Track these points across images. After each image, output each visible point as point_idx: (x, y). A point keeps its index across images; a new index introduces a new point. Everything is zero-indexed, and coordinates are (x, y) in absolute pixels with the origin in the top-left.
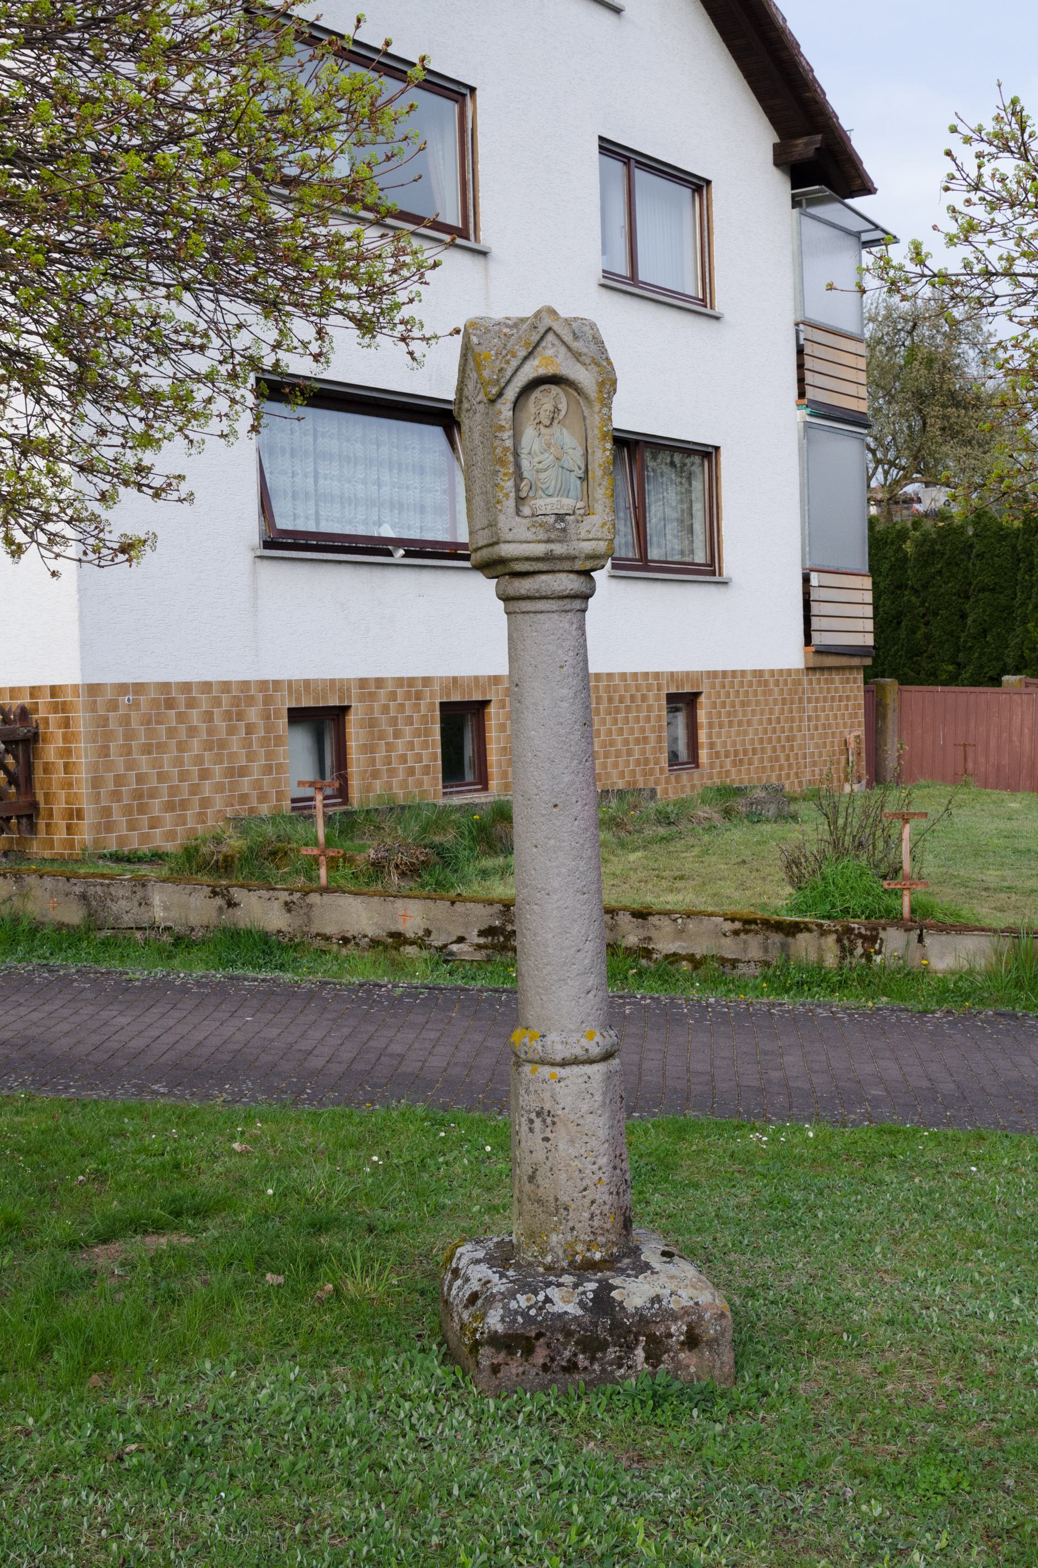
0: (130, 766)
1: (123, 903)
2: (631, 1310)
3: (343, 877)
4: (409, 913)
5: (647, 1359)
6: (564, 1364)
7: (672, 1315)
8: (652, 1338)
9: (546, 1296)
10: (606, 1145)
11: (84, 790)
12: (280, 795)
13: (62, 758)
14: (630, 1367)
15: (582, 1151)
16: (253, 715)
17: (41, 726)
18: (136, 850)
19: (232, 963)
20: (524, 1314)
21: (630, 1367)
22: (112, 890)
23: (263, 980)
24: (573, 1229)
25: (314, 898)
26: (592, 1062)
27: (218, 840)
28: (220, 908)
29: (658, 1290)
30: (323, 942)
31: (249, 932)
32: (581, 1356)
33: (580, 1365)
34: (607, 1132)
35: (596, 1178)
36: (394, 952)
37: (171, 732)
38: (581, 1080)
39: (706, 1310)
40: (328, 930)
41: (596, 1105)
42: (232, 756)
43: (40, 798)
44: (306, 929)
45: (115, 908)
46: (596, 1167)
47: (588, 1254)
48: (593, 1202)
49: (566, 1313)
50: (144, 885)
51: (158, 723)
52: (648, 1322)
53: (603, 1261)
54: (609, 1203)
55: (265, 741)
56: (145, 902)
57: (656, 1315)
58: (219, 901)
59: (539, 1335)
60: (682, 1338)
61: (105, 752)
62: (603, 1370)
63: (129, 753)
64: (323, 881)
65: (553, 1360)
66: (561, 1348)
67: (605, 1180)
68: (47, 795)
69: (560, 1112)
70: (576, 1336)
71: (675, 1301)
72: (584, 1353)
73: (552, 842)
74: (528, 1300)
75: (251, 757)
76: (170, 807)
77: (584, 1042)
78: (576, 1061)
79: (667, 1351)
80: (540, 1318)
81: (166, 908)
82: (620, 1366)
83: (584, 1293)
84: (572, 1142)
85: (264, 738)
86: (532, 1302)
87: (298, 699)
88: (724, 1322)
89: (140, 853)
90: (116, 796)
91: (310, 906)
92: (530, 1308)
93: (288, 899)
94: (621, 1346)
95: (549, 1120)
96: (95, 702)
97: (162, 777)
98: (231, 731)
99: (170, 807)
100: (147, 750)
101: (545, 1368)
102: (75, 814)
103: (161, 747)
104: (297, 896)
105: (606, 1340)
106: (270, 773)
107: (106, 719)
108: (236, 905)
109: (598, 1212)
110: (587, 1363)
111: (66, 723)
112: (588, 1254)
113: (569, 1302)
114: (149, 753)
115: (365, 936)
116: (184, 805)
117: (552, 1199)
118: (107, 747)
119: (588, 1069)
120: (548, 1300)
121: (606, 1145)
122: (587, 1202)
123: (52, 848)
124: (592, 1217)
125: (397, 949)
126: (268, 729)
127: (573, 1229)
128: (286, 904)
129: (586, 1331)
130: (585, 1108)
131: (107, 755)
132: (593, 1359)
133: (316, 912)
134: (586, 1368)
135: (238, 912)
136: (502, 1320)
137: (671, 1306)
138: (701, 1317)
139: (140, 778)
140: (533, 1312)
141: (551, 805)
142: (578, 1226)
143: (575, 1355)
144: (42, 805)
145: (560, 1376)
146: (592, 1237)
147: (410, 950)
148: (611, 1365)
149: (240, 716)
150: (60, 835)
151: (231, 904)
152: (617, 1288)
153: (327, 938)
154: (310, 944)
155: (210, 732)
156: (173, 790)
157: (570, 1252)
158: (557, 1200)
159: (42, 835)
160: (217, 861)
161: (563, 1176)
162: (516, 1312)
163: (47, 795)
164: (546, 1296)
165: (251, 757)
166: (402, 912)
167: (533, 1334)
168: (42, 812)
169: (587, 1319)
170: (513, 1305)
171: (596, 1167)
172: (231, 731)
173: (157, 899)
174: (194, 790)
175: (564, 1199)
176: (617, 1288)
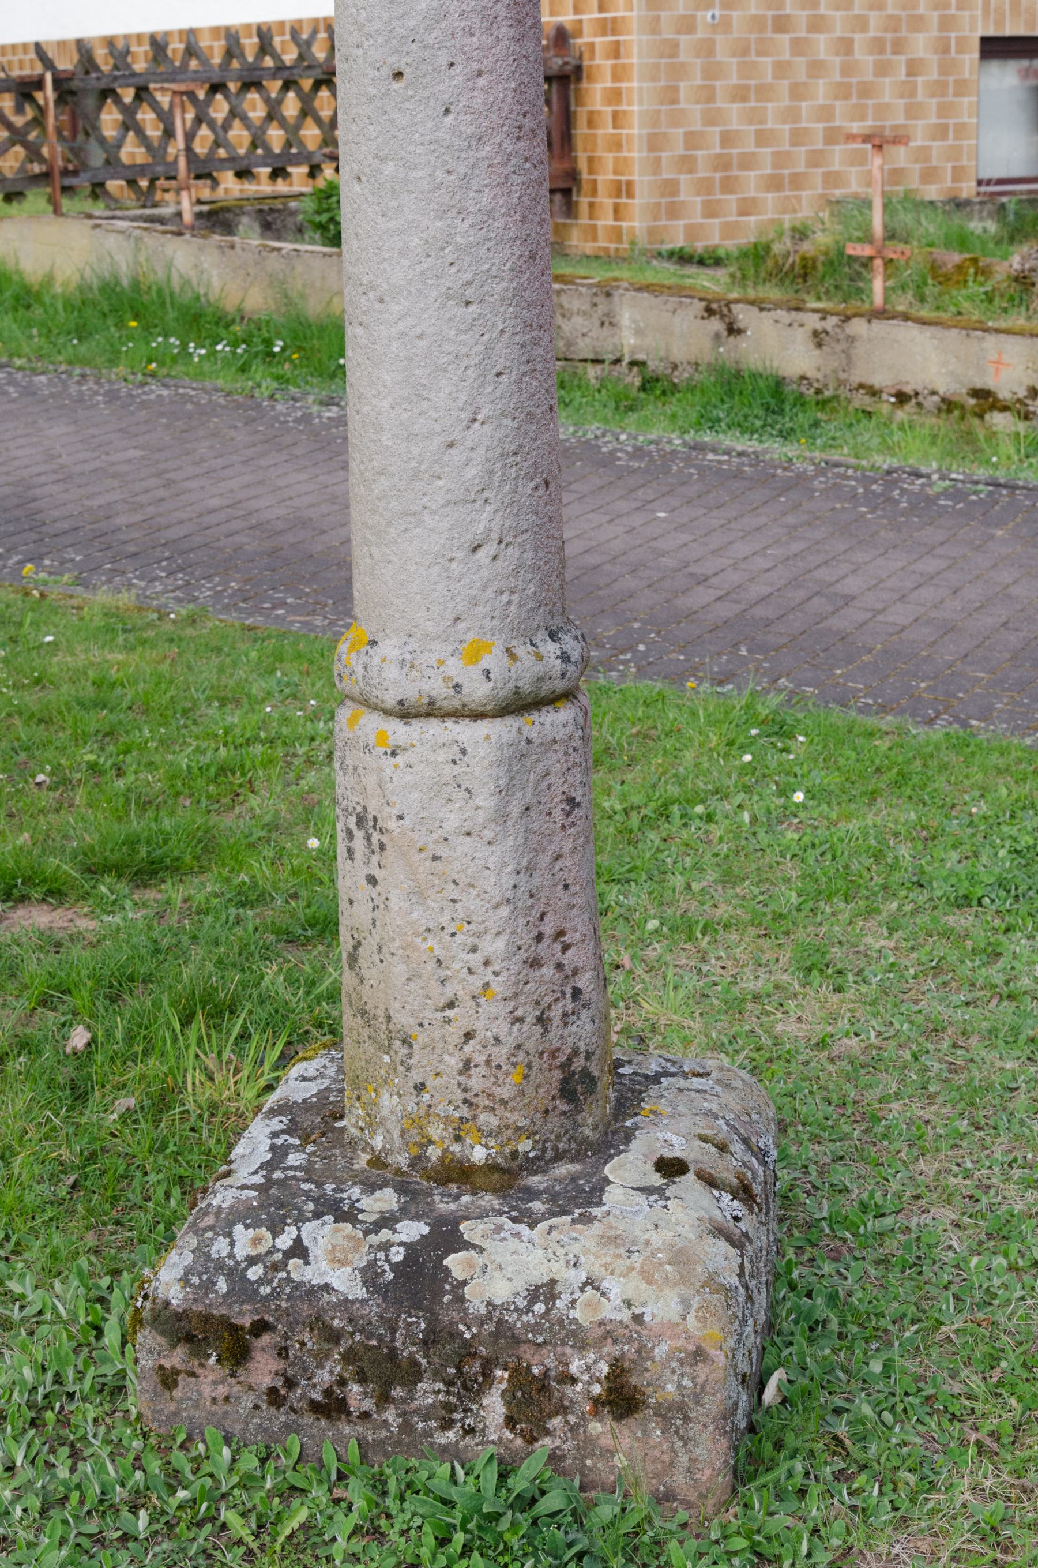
0: (711, 118)
1: (578, 320)
2: (476, 1306)
3: (970, 298)
4: (1005, 358)
5: (510, 1422)
6: (317, 1396)
7: (574, 1334)
8: (520, 1375)
9: (298, 1241)
10: (505, 911)
11: (636, 154)
12: (958, 173)
13: (610, 104)
14: (470, 1431)
15: (444, 919)
16: (921, 45)
17: (586, 56)
18: (717, 246)
19: (714, 424)
20: (235, 1274)
21: (470, 1431)
22: (564, 300)
23: (741, 454)
24: (420, 1087)
25: (858, 327)
26: (478, 716)
27: (801, 234)
28: (717, 336)
29: (559, 1270)
30: (867, 399)
31: (755, 376)
32: (355, 1388)
33: (353, 1405)
34: (508, 881)
35: (476, 983)
36: (976, 421)
37: (781, 69)
38: (443, 756)
39: (659, 1338)
40: (877, 380)
41: (481, 817)
42: (882, 110)
43: (583, 165)
44: (843, 376)
45: (567, 327)
46: (476, 959)
47: (456, 1148)
48: (468, 1036)
49: (327, 1288)
50: (608, 295)
51: (759, 53)
52: (516, 1341)
53: (492, 1168)
54: (510, 1042)
55: (939, 88)
56: (608, 322)
57: (536, 1328)
58: (716, 325)
59: (261, 1327)
60: (597, 1389)
61: (671, 95)
62: (407, 1427)
63: (711, 99)
64: (878, 299)
65: (290, 1383)
66: (311, 1363)
67: (499, 987)
68: (591, 160)
69: (392, 824)
70: (345, 1344)
71: (588, 1304)
72: (362, 1380)
73: (389, 168)
74: (256, 1241)
75: (913, 111)
76: (774, 183)
77: (454, 668)
78: (431, 711)
79: (563, 1410)
80: (265, 1290)
81: (639, 332)
82: (447, 1425)
83: (386, 1247)
84: (419, 895)
85: (937, 82)
86: (262, 1249)
87: (999, 23)
88: (702, 1371)
89: (721, 252)
90: (687, 163)
91: (851, 339)
92: (252, 1261)
93: (819, 326)
94: (450, 1383)
95: (375, 837)
96: (658, 19)
97: (762, 138)
98: (882, 69)
99: (774, 183)
100: (740, 94)
101: (275, 1398)
102: (624, 189)
103: (764, 92)
104: (832, 321)
105: (414, 1363)
106: (944, 137)
107: (675, 46)
108: (740, 332)
109: (480, 1059)
110: (368, 1405)
111: (616, 51)
112: (456, 1148)
113: (342, 1263)
114: (744, 99)
115: (934, 393)
116: (797, 181)
117: (380, 1012)
118: (676, 89)
119: (466, 732)
120: (299, 1250)
121: (505, 911)
122: (454, 1032)
123: (595, 239)
124: (467, 1065)
125: (981, 416)
126: (945, 69)
127: (420, 1087)
128: (815, 334)
129: (370, 1336)
130: (453, 821)
131: (675, 101)
132: (384, 1399)
133: (860, 350)
134: (365, 1415)
135: (743, 344)
136: (185, 1280)
137: (576, 1314)
138: (643, 1353)
139: (727, 139)
140: (254, 1273)
141: (386, 72)
142: (431, 1083)
143: (342, 1382)
144: (585, 176)
145: (308, 1419)
146: (465, 1112)
147: (999, 420)
148: (426, 1418)
149: (898, 47)
150: (606, 221)
151: (733, 330)
152: (468, 1246)
153: (874, 392)
154: (849, 401)
155: (847, 70)
156: (780, 159)
157: (414, 1135)
158: (389, 1018)
159: (584, 220)
160: (793, 266)
161: (399, 970)
162: (220, 1266)
163: (591, 160)
164: (298, 1241)
165: (913, 111)
166: (994, 357)
167: (246, 1322)
168: (585, 186)
169: (373, 1310)
170: (220, 1247)
171: (476, 959)
172: (882, 69)
173: (626, 317)
174: (815, 159)
175: (403, 1020)
176: (468, 1246)
